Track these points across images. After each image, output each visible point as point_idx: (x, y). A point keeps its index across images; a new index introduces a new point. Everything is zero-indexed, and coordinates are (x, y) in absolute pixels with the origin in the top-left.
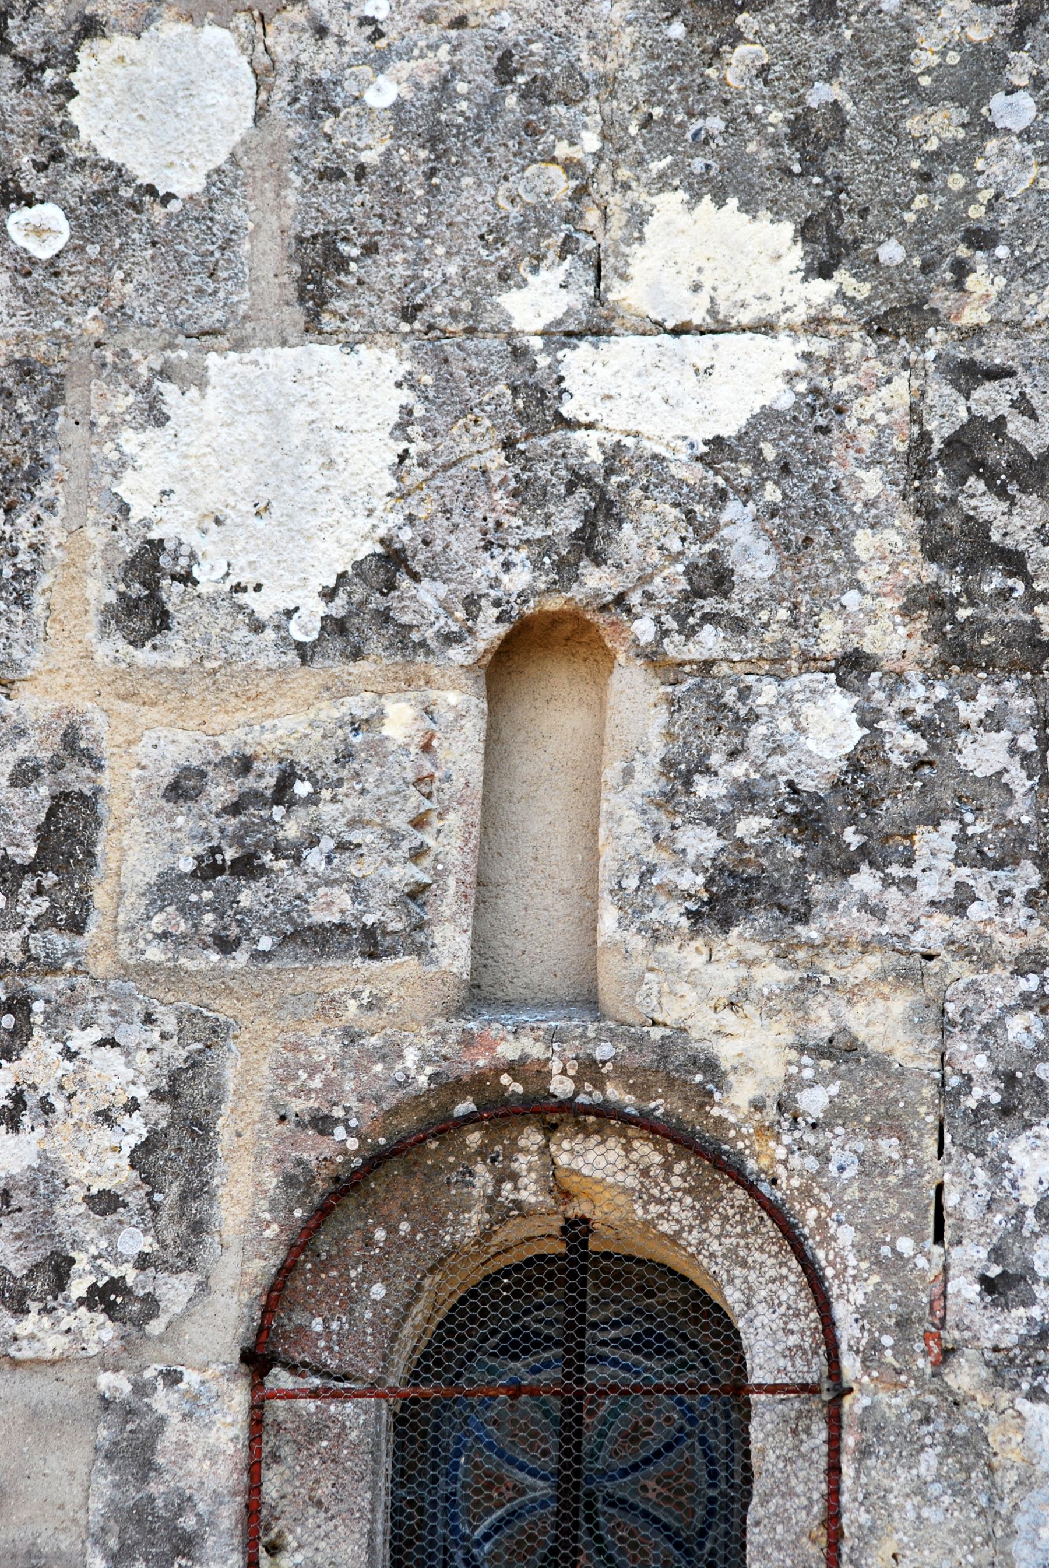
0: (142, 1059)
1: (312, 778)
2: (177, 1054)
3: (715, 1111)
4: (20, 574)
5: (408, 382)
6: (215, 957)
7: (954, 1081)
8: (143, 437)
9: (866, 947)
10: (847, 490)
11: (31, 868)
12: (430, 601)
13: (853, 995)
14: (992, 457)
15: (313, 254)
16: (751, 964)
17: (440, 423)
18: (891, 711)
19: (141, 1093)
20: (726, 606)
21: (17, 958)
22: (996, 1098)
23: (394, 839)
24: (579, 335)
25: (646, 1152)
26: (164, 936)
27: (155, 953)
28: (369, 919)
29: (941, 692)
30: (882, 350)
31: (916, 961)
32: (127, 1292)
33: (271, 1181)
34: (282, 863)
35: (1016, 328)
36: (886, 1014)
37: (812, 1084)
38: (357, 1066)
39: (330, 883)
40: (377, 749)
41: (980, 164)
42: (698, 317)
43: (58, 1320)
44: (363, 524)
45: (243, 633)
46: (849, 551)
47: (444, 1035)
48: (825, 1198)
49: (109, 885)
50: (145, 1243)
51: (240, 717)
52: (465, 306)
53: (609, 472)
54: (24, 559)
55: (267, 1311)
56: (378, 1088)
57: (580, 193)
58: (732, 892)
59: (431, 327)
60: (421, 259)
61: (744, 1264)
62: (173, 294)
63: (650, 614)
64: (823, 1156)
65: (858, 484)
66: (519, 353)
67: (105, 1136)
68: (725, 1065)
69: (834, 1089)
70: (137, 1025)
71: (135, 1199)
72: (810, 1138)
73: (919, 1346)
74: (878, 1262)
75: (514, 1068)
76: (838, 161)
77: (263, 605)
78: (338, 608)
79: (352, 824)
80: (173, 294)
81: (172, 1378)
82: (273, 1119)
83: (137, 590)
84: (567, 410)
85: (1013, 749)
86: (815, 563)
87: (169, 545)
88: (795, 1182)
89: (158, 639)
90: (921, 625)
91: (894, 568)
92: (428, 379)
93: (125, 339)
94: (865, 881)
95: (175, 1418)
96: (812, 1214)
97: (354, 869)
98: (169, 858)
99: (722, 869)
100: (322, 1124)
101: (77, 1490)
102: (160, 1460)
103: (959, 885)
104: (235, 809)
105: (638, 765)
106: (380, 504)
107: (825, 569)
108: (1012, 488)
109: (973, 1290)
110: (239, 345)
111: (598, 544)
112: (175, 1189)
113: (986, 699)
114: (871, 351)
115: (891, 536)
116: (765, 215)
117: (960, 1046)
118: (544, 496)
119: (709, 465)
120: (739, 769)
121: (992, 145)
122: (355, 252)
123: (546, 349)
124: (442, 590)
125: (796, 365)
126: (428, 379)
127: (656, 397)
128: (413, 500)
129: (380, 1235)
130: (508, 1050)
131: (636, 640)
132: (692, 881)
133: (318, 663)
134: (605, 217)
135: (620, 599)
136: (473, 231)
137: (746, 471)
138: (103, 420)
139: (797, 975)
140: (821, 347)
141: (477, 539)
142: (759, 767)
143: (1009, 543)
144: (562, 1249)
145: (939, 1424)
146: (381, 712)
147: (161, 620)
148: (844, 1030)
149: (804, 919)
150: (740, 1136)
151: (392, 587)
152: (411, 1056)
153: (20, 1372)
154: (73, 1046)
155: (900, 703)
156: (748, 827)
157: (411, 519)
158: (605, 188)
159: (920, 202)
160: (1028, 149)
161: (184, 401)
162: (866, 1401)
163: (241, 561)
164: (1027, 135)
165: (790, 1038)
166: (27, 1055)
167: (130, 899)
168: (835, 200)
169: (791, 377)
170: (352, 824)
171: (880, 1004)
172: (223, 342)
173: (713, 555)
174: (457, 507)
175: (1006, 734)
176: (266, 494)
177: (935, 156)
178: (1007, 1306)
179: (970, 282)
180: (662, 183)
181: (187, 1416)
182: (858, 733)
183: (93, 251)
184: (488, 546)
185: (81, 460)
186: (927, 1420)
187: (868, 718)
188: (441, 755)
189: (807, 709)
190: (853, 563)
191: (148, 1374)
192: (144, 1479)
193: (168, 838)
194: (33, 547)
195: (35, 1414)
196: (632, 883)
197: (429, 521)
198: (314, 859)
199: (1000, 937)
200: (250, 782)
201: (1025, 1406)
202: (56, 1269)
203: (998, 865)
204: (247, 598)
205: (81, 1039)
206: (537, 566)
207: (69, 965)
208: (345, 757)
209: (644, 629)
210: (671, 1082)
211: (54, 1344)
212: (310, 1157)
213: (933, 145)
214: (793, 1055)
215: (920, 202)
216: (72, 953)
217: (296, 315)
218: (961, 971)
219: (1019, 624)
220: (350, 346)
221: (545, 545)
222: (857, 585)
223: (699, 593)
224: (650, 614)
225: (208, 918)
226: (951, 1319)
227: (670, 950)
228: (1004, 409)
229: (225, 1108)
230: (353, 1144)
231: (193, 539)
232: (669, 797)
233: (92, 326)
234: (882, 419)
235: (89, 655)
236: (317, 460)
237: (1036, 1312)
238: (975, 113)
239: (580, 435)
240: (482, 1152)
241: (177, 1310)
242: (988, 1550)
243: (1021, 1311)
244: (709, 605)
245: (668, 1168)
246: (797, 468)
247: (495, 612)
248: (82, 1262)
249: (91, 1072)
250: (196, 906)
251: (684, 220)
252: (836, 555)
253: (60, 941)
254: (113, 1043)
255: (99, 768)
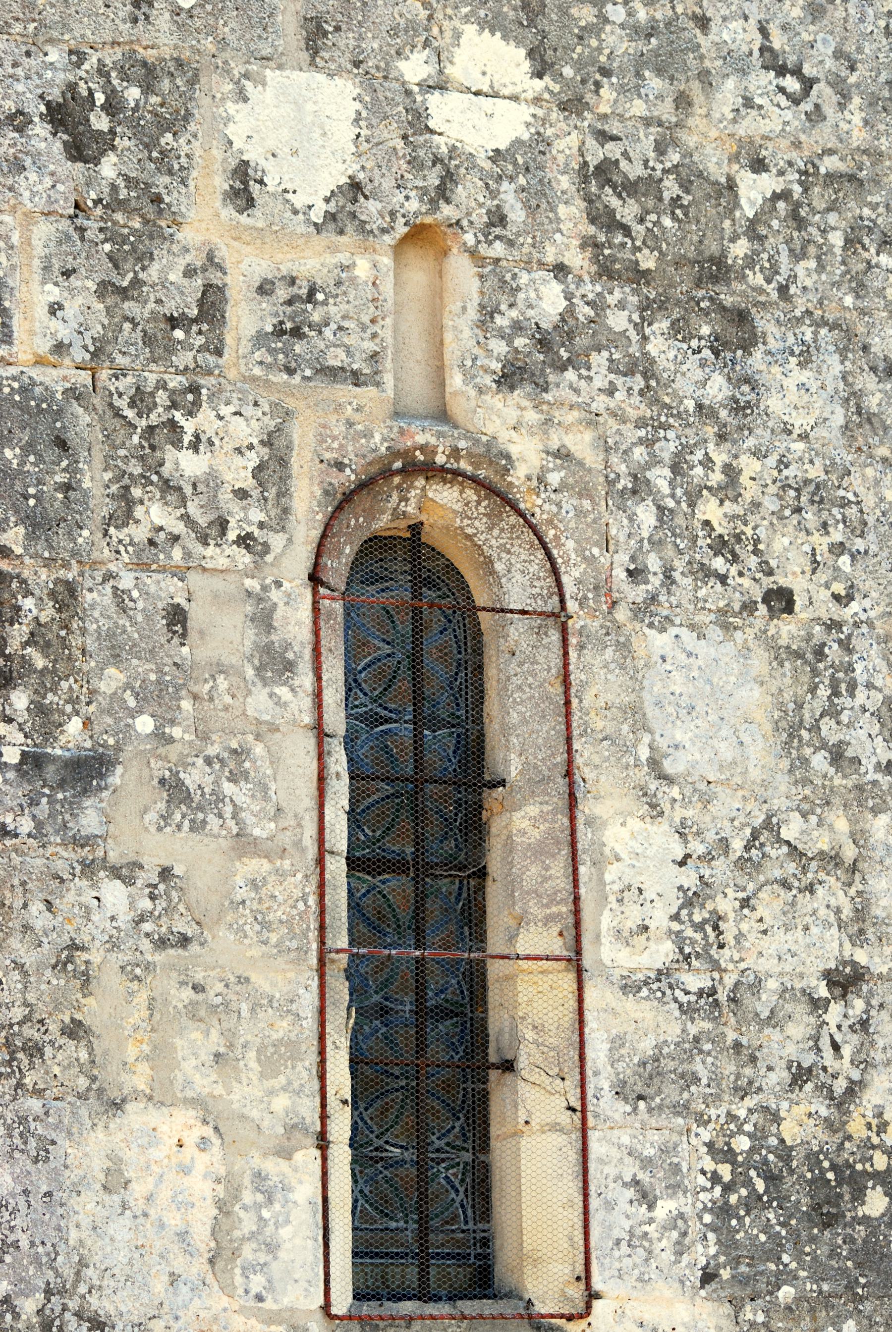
0: (253, 422)
1: (324, 292)
2: (272, 424)
3: (509, 479)
4: (182, 168)
5: (358, 98)
6: (286, 377)
7: (612, 476)
8: (237, 107)
9: (571, 407)
10: (554, 184)
11: (195, 321)
12: (374, 210)
13: (568, 429)
14: (615, 178)
15: (312, 26)
16: (522, 409)
17: (374, 122)
18: (578, 294)
19: (255, 441)
20: (504, 232)
21: (192, 366)
22: (630, 486)
23: (364, 328)
24: (434, 88)
25: (470, 494)
26: (261, 363)
27: (257, 371)
28: (355, 367)
29: (598, 288)
30: (566, 118)
31: (593, 416)
32: (254, 539)
33: (318, 492)
34: (313, 333)
35: (621, 118)
36: (582, 439)
37: (553, 470)
38: (353, 439)
39: (335, 346)
40: (353, 280)
41: (603, 36)
42: (486, 88)
43: (223, 551)
44: (341, 167)
45: (289, 214)
46: (556, 214)
47: (391, 428)
48: (560, 525)
49: (233, 333)
50: (262, 517)
51: (289, 256)
52: (382, 65)
53: (450, 158)
54: (183, 160)
55: (318, 555)
56: (364, 450)
57: (430, 18)
58: (514, 373)
59: (367, 73)
60: (361, 38)
61: (509, 552)
62: (248, 36)
63: (472, 232)
64: (559, 505)
65: (559, 182)
66: (408, 93)
67: (238, 461)
68: (514, 457)
69: (563, 474)
70: (251, 407)
71: (255, 493)
72: (553, 496)
73: (603, 599)
74: (585, 558)
75: (422, 448)
76: (542, 23)
77: (299, 201)
78: (332, 207)
79: (344, 317)
80: (248, 36)
81: (278, 584)
82: (317, 461)
83: (238, 185)
84: (431, 124)
85: (630, 320)
86: (541, 217)
87: (252, 164)
88: (545, 516)
89: (250, 211)
90: (588, 254)
91: (575, 225)
92: (367, 99)
93: (227, 55)
94: (570, 375)
95: (281, 605)
96: (552, 532)
97: (346, 340)
98: (260, 324)
99: (508, 361)
100: (340, 466)
101: (238, 635)
102: (275, 624)
103: (611, 382)
104: (289, 302)
105: (469, 306)
106: (349, 158)
107: (546, 221)
108: (624, 194)
109: (624, 575)
110: (280, 67)
111: (448, 193)
112: (274, 491)
113: (617, 295)
114: (561, 118)
115: (573, 209)
116: (512, 42)
117: (614, 459)
118: (422, 166)
119: (494, 162)
120: (514, 313)
121: (608, 28)
122: (331, 29)
123: (420, 92)
124: (379, 206)
125: (531, 120)
126: (367, 99)
127: (470, 124)
128: (364, 158)
129: (353, 522)
130: (420, 439)
131: (465, 244)
132: (496, 366)
133: (324, 234)
134: (441, 32)
135: (458, 222)
136: (384, 28)
137: (510, 167)
138: (219, 96)
139: (543, 417)
140: (540, 113)
141: (393, 183)
142: (523, 314)
143: (624, 221)
144: (408, 535)
145: (613, 636)
146: (354, 263)
147: (250, 202)
148: (564, 446)
149: (546, 390)
150: (519, 492)
151: (356, 201)
152: (377, 438)
153: (206, 575)
154: (222, 414)
155: (582, 291)
156: (520, 342)
157: (363, 167)
158: (441, 17)
159: (579, 49)
160: (623, 33)
161: (256, 91)
162: (582, 623)
163: (286, 177)
164: (622, 26)
165: (541, 447)
166: (199, 415)
167: (244, 342)
168: (542, 42)
169: (528, 125)
170: (344, 317)
171: (579, 436)
172: (272, 64)
173: (498, 206)
174: (384, 164)
175: (626, 313)
176: (296, 145)
177: (582, 29)
178: (638, 584)
179: (602, 91)
180: (466, 19)
181: (287, 604)
182: (565, 303)
183: (209, 8)
184: (398, 187)
185: (209, 114)
186: (608, 634)
187: (569, 296)
188: (381, 288)
189: (542, 288)
190: (558, 220)
191: (268, 581)
192: (269, 632)
193: (259, 313)
194: (188, 156)
195: (216, 596)
196: (469, 363)
197: (372, 170)
198: (328, 332)
199: (629, 409)
200: (295, 290)
201: (647, 631)
202: (221, 525)
203: (625, 375)
204: (289, 196)
205: (226, 411)
206: (421, 201)
207: (217, 372)
208: (338, 284)
209: (469, 239)
210: (491, 462)
211: (222, 562)
212: (335, 481)
213: (583, 23)
214: (544, 455)
215: (579, 49)
216: (217, 366)
217: (305, 56)
218: (613, 425)
219: (631, 261)
220: (331, 76)
221: (423, 190)
222: (559, 231)
223: (492, 224)
224: (472, 232)
225: (281, 356)
226: (614, 588)
227: (487, 398)
228: (618, 156)
229: (294, 453)
230: (353, 477)
231: (262, 163)
232: (483, 322)
233: (210, 46)
234: (568, 152)
235: (218, 215)
236: (319, 132)
237: (649, 587)
238: (600, 11)
239: (436, 137)
240: (399, 487)
241: (279, 551)
242: (633, 696)
243: (643, 587)
244: (497, 231)
245: (479, 503)
246: (532, 169)
247: (403, 220)
248: (232, 523)
249: (231, 428)
250: (275, 350)
251: (477, 39)
252: (551, 215)
253: (211, 359)
254: (241, 415)
255: (225, 273)
